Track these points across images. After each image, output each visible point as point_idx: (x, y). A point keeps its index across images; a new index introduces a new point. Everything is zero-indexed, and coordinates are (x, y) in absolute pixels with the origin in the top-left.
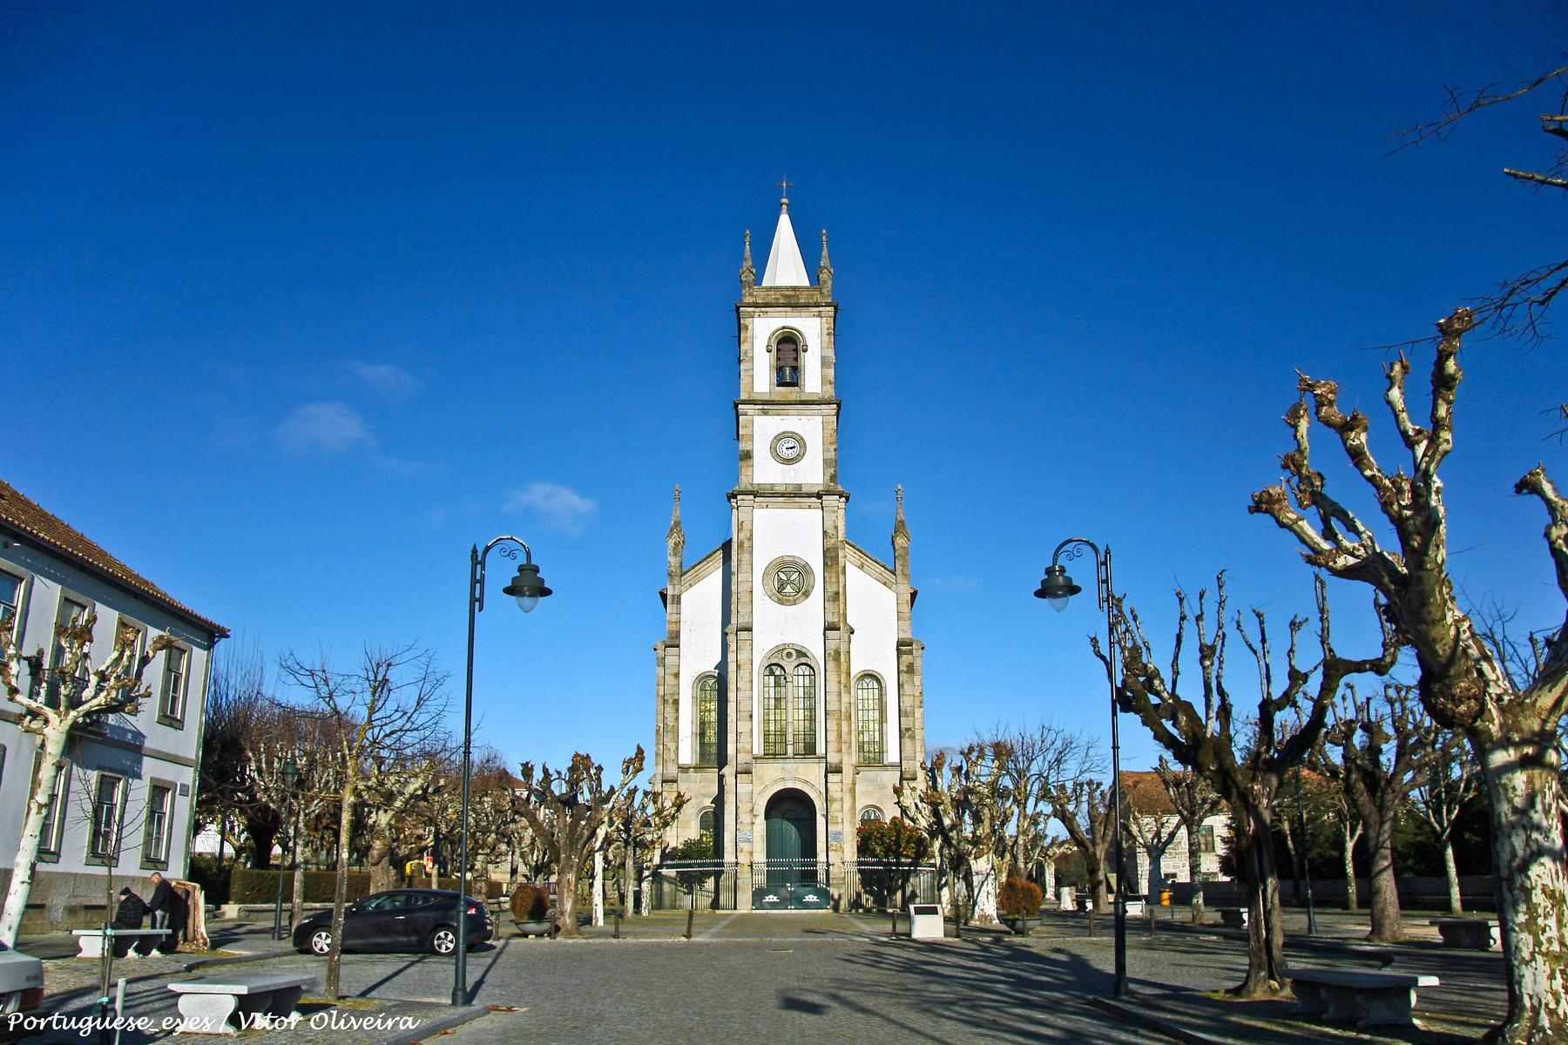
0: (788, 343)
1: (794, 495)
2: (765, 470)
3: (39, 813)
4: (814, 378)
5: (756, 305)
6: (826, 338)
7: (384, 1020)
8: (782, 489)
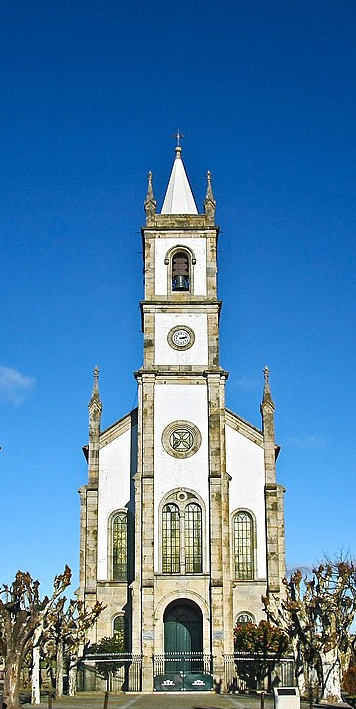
1: (186, 373)
2: (163, 355)
4: (201, 285)
8: (177, 370)
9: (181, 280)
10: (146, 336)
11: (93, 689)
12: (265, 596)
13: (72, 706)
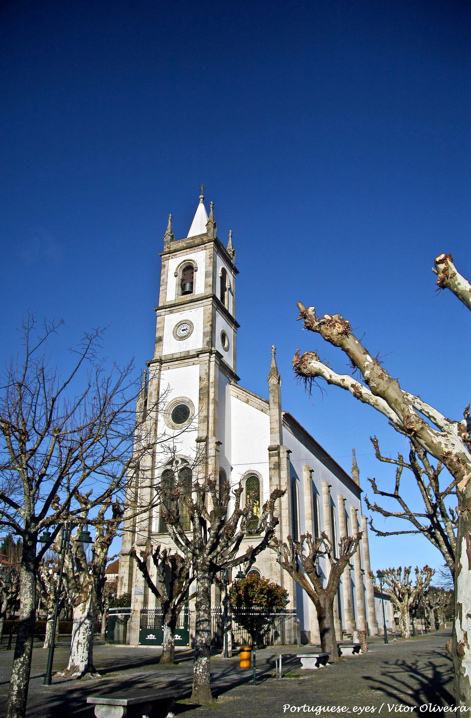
0: (189, 269)
1: (185, 358)
2: (170, 346)
3: (64, 587)
4: (200, 286)
5: (170, 253)
6: (209, 261)
7: (453, 708)
8: (178, 356)
9: (186, 285)
10: (158, 335)
11: (125, 642)
12: (377, 533)
13: (142, 697)
